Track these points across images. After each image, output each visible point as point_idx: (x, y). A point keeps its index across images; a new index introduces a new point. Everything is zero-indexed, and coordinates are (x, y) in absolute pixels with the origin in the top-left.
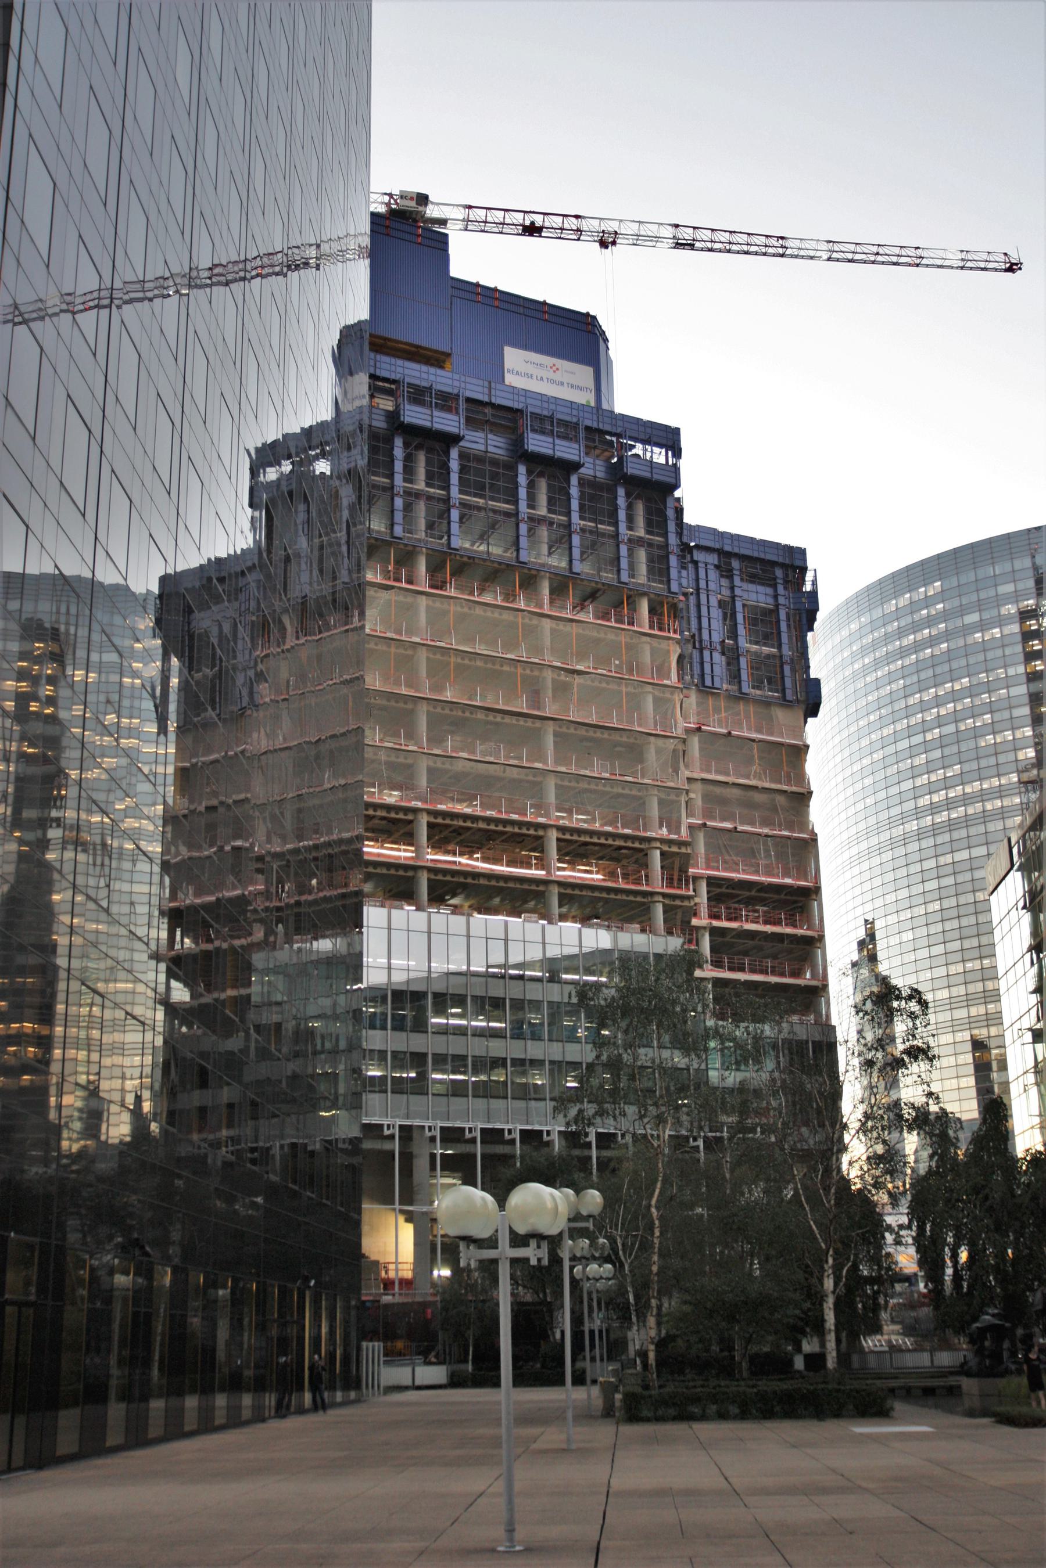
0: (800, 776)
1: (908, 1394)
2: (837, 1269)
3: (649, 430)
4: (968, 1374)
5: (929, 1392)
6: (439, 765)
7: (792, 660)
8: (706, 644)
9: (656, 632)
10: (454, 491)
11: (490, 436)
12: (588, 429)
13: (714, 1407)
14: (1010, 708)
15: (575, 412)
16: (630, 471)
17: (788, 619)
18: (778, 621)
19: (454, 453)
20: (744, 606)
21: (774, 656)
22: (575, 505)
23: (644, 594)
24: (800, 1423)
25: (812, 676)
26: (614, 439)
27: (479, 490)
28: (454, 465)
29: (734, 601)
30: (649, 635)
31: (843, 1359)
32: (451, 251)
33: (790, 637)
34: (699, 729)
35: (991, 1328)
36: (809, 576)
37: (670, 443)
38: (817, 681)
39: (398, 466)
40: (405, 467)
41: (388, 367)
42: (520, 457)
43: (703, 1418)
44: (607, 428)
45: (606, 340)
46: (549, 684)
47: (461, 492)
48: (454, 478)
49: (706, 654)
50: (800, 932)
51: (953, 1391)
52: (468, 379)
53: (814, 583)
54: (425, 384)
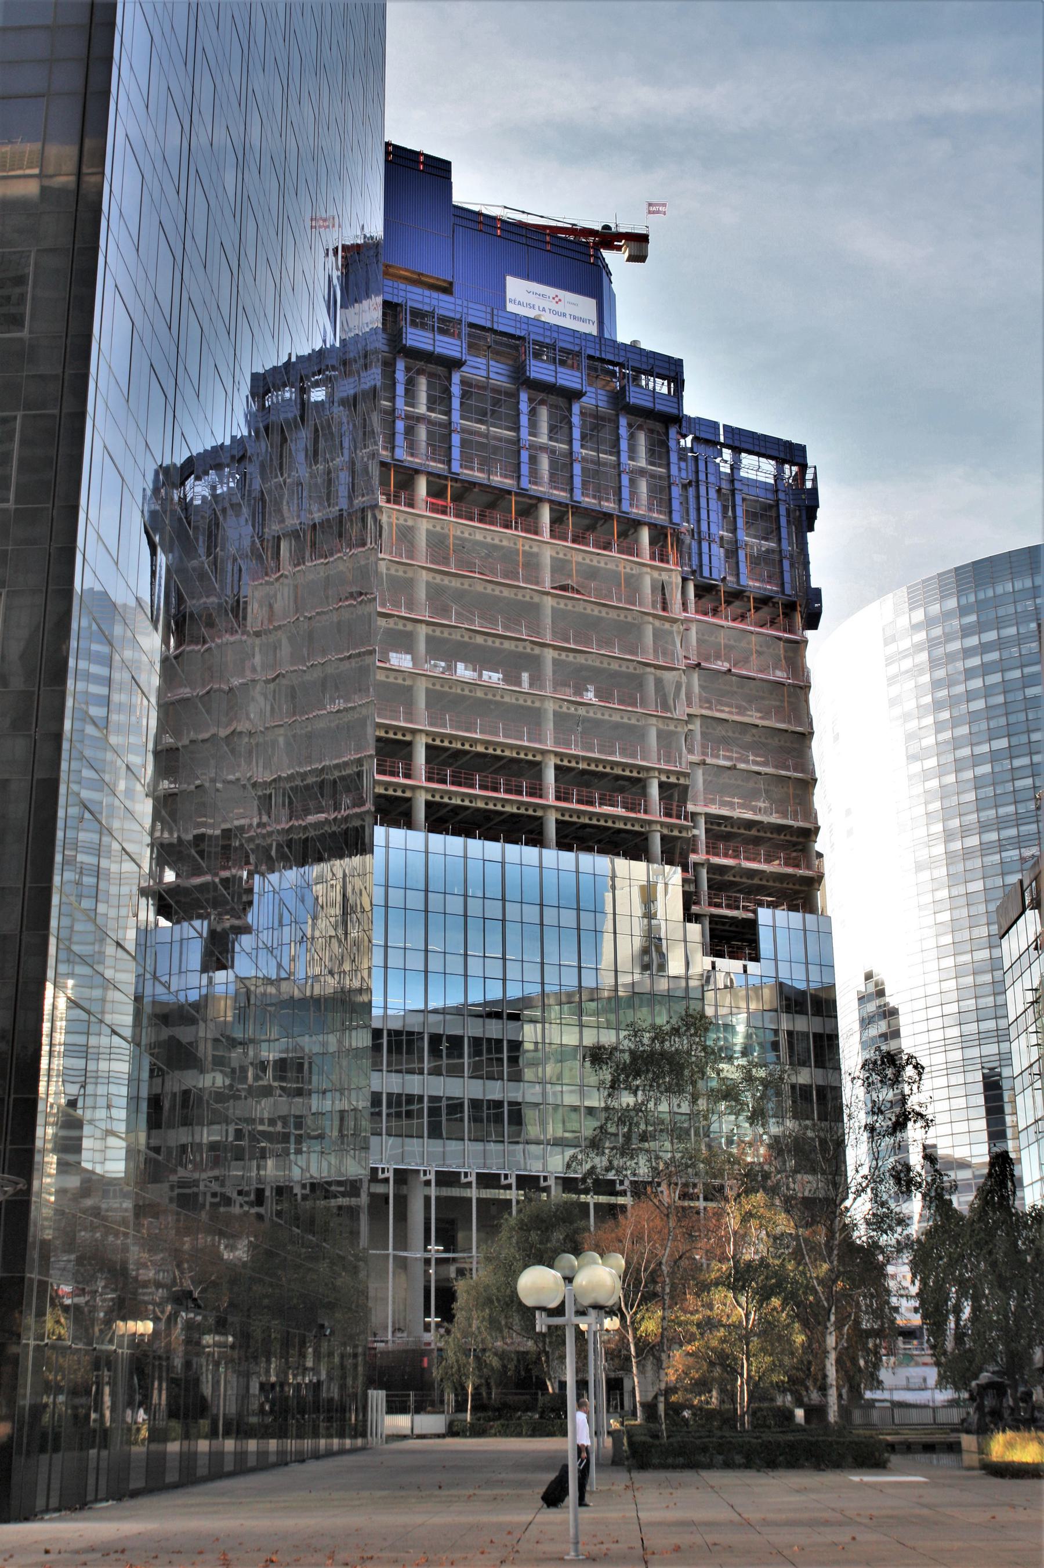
0: (809, 813)
1: (908, 1448)
2: (839, 1327)
3: (651, 361)
4: (968, 1432)
5: (929, 1448)
6: (438, 633)
7: (792, 556)
8: (704, 535)
9: (657, 564)
10: (456, 416)
11: (492, 363)
12: (590, 357)
13: (720, 1458)
14: (1029, 732)
15: (577, 341)
16: (633, 401)
17: (788, 515)
18: (778, 516)
19: (456, 378)
20: (744, 500)
21: (773, 551)
22: (576, 434)
23: (645, 524)
24: (801, 1472)
25: (814, 585)
26: (617, 369)
27: (482, 416)
28: (456, 390)
29: (733, 495)
30: (652, 567)
31: (845, 1412)
32: (454, 179)
33: (789, 534)
34: (699, 665)
35: (990, 1385)
36: (809, 476)
37: (673, 374)
38: (818, 591)
39: (400, 390)
40: (407, 391)
41: (390, 290)
42: (522, 384)
43: (709, 1466)
44: (610, 357)
45: (609, 274)
46: (549, 612)
47: (462, 417)
48: (456, 403)
49: (705, 545)
50: (801, 872)
51: (954, 1448)
52: (471, 305)
53: (815, 480)
54: (427, 308)
